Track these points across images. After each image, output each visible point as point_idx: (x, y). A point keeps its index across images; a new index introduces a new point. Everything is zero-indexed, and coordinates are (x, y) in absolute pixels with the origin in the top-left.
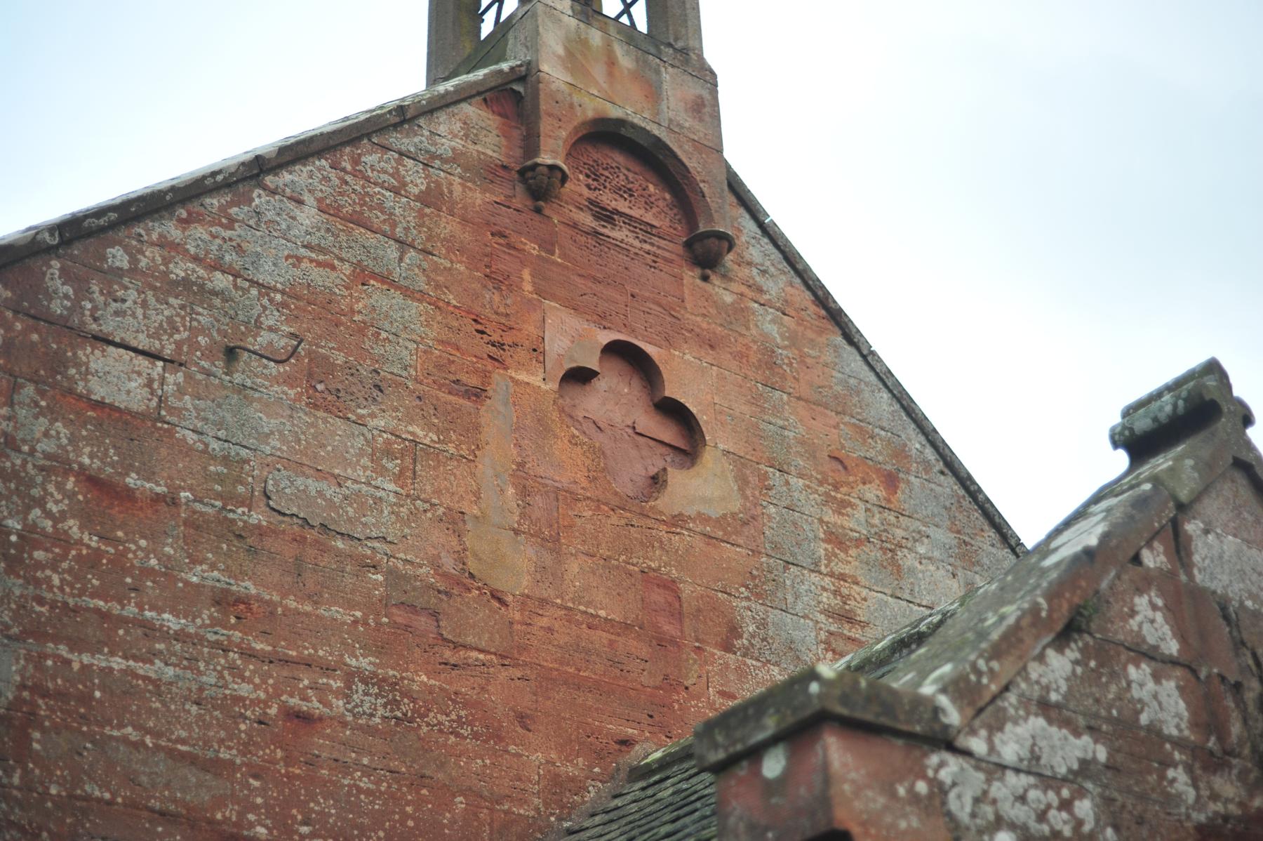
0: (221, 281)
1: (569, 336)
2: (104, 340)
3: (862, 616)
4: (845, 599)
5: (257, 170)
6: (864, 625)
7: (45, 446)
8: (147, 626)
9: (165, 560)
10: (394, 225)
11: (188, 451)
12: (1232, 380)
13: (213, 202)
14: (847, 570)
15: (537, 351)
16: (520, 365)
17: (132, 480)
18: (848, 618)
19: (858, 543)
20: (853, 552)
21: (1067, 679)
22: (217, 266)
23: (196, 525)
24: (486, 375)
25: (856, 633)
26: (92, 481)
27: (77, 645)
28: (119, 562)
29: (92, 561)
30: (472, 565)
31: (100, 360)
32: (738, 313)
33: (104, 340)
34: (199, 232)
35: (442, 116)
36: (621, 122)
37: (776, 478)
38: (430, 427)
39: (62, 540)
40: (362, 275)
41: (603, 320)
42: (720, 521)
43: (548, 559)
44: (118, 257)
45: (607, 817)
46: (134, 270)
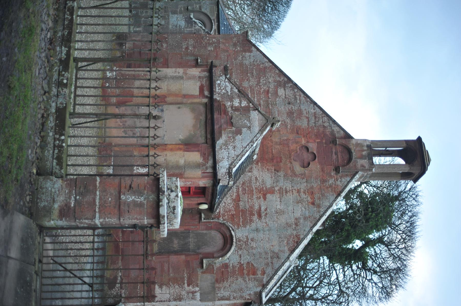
0: (298, 101)
1: (313, 147)
2: (285, 90)
3: (287, 195)
4: (289, 192)
5: (315, 104)
6: (286, 195)
7: (270, 86)
8: (254, 97)
9: (262, 99)
10: (317, 121)
11: (276, 99)
12: (427, 172)
13: (308, 100)
14: (294, 193)
15: (308, 142)
16: (305, 140)
17: (270, 94)
18: (286, 192)
19: (299, 195)
20: (297, 194)
21: (387, 267)
22: (300, 101)
23: (267, 101)
24: (301, 134)
25: (284, 194)
26: (268, 91)
27: (250, 91)
28: (260, 94)
29: (260, 92)
30: (274, 133)
31: (282, 89)
32: (331, 177)
33: (285, 90)
34: (304, 99)
35: (338, 128)
36: (352, 153)
37: (305, 180)
38: (290, 127)
39: (261, 89)
40: (308, 118)
41: (318, 152)
42: (293, 170)
43: (279, 143)
44: (296, 90)
45: (185, 100)
46: (295, 92)
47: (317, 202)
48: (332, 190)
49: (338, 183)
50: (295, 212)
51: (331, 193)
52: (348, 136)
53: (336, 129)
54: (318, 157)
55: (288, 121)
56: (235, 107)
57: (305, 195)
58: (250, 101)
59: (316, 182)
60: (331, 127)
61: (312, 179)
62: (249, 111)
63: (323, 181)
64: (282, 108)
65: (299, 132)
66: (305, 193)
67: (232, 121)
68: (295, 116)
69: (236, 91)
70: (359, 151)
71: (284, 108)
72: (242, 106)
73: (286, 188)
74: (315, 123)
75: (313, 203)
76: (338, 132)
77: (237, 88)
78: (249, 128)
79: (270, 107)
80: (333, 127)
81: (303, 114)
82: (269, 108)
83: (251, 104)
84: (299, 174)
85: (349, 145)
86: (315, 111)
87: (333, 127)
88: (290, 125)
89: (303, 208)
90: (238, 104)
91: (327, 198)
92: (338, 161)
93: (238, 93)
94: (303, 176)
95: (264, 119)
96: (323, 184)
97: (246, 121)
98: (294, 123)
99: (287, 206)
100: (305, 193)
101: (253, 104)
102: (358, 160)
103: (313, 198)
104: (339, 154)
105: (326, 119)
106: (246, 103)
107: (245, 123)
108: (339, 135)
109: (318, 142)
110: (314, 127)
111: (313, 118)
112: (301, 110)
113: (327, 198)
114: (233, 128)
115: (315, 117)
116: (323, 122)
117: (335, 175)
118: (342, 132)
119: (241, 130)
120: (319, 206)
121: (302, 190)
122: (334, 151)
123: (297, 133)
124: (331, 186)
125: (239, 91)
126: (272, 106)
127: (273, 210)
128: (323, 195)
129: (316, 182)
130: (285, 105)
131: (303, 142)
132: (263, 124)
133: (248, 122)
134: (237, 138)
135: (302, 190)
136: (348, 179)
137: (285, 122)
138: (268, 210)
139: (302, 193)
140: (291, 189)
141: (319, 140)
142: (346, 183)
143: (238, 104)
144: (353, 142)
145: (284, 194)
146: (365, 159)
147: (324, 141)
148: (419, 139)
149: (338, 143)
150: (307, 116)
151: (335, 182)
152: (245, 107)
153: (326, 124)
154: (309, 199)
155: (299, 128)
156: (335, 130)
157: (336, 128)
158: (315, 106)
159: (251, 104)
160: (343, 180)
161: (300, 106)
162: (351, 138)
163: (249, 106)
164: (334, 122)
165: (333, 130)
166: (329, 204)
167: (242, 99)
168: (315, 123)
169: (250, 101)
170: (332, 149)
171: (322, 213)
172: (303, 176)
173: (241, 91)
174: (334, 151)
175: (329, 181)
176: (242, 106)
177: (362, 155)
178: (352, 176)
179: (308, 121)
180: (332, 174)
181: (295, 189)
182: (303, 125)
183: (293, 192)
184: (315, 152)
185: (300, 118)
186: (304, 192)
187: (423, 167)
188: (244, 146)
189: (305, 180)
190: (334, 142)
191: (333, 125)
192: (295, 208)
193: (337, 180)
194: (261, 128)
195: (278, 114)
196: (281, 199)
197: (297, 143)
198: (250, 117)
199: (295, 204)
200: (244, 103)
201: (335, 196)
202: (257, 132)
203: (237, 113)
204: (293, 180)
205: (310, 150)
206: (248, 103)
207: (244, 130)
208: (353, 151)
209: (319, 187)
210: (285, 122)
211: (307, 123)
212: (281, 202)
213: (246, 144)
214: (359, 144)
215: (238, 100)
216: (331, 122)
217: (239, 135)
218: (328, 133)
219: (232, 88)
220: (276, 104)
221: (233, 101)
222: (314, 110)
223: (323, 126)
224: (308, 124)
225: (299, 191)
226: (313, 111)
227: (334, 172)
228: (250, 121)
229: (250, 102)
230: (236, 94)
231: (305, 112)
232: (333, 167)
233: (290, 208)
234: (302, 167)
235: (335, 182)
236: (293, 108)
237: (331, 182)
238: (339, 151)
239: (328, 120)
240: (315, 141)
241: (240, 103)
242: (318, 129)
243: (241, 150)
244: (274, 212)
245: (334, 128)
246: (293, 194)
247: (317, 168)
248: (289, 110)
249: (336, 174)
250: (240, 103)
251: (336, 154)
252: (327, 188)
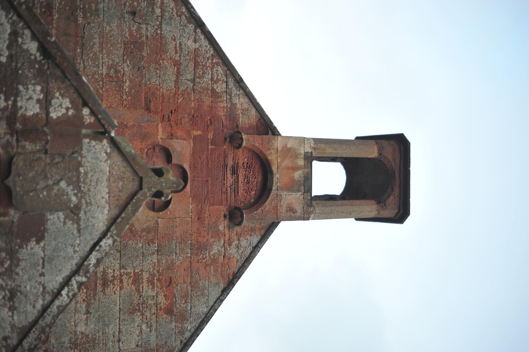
0: (158, 11)
1: (182, 149)
3: (108, 291)
4: (112, 281)
5: (200, 24)
6: (103, 291)
14: (125, 284)
15: (171, 136)
16: (164, 129)
18: (105, 284)
19: (138, 290)
20: (133, 288)
22: (163, 11)
24: (156, 113)
32: (217, 234)
35: (247, 100)
37: (154, 247)
38: (130, 89)
40: (177, 64)
41: (193, 166)
47: (180, 304)
48: (216, 271)
49: (232, 251)
50: (123, 338)
51: (213, 280)
52: (266, 127)
53: (241, 102)
54: (193, 181)
55: (126, 68)
56: (25, 119)
57: (153, 288)
58: (82, 98)
59: (182, 250)
60: (230, 95)
61: (174, 242)
62: (78, 139)
63: (199, 248)
64: (114, 25)
65: (152, 108)
66: (153, 284)
67: (9, 182)
68: (145, 54)
69: (33, 47)
70: (289, 168)
71: (119, 26)
72: (54, 115)
73: (104, 271)
74: (193, 81)
75: (169, 311)
76: (245, 111)
77: (34, 37)
78: (74, 213)
79: (80, 20)
80: (236, 95)
81: (165, 51)
82: (76, 21)
83: (86, 111)
84: (143, 230)
85: (268, 152)
86: (197, 45)
87: (236, 95)
88: (131, 81)
89: (144, 327)
90: (37, 109)
91: (203, 295)
92: (236, 191)
93: (39, 57)
94: (150, 236)
95: (129, 174)
96: (197, 255)
97: (63, 184)
98: (142, 76)
99: (104, 324)
100: (153, 284)
101: (93, 113)
102: (284, 193)
103: (170, 297)
104: (241, 172)
105: (220, 70)
106: (67, 103)
107: (62, 192)
108: (246, 121)
109: (195, 138)
110: (189, 94)
111: (191, 67)
112: (162, 37)
113: (203, 295)
114: (12, 212)
115: (196, 65)
116: (212, 79)
117: (227, 231)
118: (253, 111)
119: (42, 221)
120: (183, 318)
121: (146, 276)
122: (230, 163)
123: (148, 109)
124: (214, 261)
125: (43, 49)
126: (85, 17)
127: (66, 339)
128: (194, 285)
129: (182, 250)
130: (123, 17)
131: (161, 135)
132: (124, 196)
133: (70, 190)
134: (24, 253)
135: (146, 276)
136: (255, 240)
137: (117, 72)
138: (53, 341)
139: (145, 284)
140: (117, 273)
141: (199, 133)
142: (249, 251)
143: (37, 109)
144: (278, 143)
145: (99, 288)
146: (298, 191)
147: (210, 136)
148: (400, 144)
149: (244, 144)
150: (177, 58)
151: (225, 249)
152: (64, 121)
153: (220, 88)
154: (161, 299)
155: (153, 93)
156: (239, 106)
157: (242, 100)
158: (198, 30)
159: (86, 111)
160: (244, 243)
161: (160, 27)
162: (275, 132)
163: (79, 117)
164: (239, 82)
165: (234, 105)
166: (206, 310)
167: (53, 85)
168: (193, 81)
169: (82, 98)
170: (226, 157)
171: (188, 335)
172: (150, 236)
173: (53, 51)
174: (230, 163)
175: (211, 246)
176: (54, 115)
177: (292, 179)
178: (263, 232)
179: (178, 74)
180: (221, 228)
181: (128, 274)
182: (165, 86)
183: (121, 281)
184: (186, 166)
185: (157, 63)
186: (151, 282)
187: (401, 212)
188: (53, 283)
189: (154, 247)
190: (234, 139)
191: (235, 91)
192: (123, 328)
193: (230, 245)
194: (115, 212)
195: (101, 44)
196: (88, 306)
197: (144, 137)
198: (80, 165)
199: (126, 317)
200: (61, 107)
201: (222, 286)
202: (101, 226)
203: (29, 146)
204: (126, 246)
205: (174, 161)
206: (74, 105)
207: (55, 219)
208: (274, 168)
209: (186, 264)
210: (117, 72)
211: (174, 78)
212: (88, 312)
213: (60, 279)
214: (290, 150)
215: (36, 91)
216: (231, 84)
217: (33, 243)
218: (221, 113)
219: (14, 34)
220: (97, 10)
221: (17, 93)
222: (195, 41)
223: (213, 90)
224: (176, 82)
225: (137, 280)
226: (191, 44)
227: (226, 222)
228: (76, 184)
229: (85, 104)
230: (32, 63)
231: (171, 47)
232: (223, 209)
233: (112, 329)
234: (149, 208)
235: (225, 249)
236: (143, 31)
237: (215, 249)
238: (241, 162)
239: (226, 75)
240: (188, 134)
241: (46, 103)
242: (200, 100)
243: (39, 305)
244: (67, 345)
245: (236, 100)
246: (121, 288)
247: (187, 213)
248: (131, 34)
249: (229, 228)
250: (46, 103)
251: (234, 171)
252: (206, 265)
